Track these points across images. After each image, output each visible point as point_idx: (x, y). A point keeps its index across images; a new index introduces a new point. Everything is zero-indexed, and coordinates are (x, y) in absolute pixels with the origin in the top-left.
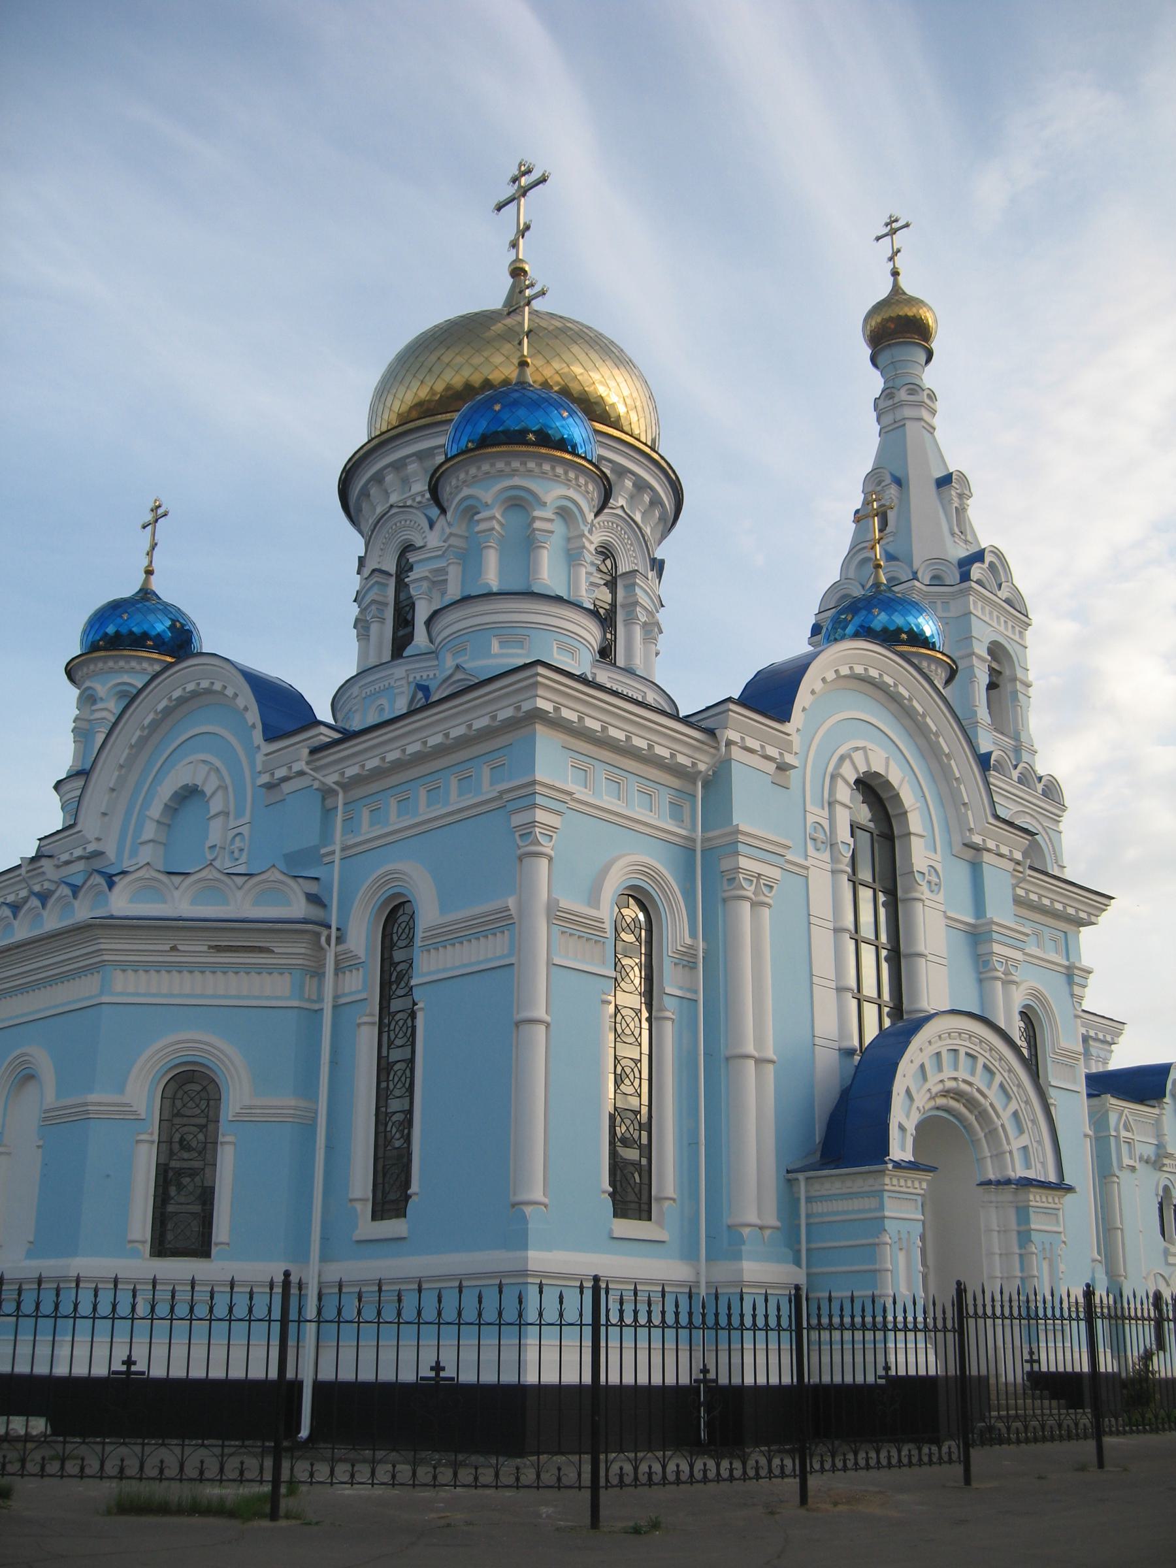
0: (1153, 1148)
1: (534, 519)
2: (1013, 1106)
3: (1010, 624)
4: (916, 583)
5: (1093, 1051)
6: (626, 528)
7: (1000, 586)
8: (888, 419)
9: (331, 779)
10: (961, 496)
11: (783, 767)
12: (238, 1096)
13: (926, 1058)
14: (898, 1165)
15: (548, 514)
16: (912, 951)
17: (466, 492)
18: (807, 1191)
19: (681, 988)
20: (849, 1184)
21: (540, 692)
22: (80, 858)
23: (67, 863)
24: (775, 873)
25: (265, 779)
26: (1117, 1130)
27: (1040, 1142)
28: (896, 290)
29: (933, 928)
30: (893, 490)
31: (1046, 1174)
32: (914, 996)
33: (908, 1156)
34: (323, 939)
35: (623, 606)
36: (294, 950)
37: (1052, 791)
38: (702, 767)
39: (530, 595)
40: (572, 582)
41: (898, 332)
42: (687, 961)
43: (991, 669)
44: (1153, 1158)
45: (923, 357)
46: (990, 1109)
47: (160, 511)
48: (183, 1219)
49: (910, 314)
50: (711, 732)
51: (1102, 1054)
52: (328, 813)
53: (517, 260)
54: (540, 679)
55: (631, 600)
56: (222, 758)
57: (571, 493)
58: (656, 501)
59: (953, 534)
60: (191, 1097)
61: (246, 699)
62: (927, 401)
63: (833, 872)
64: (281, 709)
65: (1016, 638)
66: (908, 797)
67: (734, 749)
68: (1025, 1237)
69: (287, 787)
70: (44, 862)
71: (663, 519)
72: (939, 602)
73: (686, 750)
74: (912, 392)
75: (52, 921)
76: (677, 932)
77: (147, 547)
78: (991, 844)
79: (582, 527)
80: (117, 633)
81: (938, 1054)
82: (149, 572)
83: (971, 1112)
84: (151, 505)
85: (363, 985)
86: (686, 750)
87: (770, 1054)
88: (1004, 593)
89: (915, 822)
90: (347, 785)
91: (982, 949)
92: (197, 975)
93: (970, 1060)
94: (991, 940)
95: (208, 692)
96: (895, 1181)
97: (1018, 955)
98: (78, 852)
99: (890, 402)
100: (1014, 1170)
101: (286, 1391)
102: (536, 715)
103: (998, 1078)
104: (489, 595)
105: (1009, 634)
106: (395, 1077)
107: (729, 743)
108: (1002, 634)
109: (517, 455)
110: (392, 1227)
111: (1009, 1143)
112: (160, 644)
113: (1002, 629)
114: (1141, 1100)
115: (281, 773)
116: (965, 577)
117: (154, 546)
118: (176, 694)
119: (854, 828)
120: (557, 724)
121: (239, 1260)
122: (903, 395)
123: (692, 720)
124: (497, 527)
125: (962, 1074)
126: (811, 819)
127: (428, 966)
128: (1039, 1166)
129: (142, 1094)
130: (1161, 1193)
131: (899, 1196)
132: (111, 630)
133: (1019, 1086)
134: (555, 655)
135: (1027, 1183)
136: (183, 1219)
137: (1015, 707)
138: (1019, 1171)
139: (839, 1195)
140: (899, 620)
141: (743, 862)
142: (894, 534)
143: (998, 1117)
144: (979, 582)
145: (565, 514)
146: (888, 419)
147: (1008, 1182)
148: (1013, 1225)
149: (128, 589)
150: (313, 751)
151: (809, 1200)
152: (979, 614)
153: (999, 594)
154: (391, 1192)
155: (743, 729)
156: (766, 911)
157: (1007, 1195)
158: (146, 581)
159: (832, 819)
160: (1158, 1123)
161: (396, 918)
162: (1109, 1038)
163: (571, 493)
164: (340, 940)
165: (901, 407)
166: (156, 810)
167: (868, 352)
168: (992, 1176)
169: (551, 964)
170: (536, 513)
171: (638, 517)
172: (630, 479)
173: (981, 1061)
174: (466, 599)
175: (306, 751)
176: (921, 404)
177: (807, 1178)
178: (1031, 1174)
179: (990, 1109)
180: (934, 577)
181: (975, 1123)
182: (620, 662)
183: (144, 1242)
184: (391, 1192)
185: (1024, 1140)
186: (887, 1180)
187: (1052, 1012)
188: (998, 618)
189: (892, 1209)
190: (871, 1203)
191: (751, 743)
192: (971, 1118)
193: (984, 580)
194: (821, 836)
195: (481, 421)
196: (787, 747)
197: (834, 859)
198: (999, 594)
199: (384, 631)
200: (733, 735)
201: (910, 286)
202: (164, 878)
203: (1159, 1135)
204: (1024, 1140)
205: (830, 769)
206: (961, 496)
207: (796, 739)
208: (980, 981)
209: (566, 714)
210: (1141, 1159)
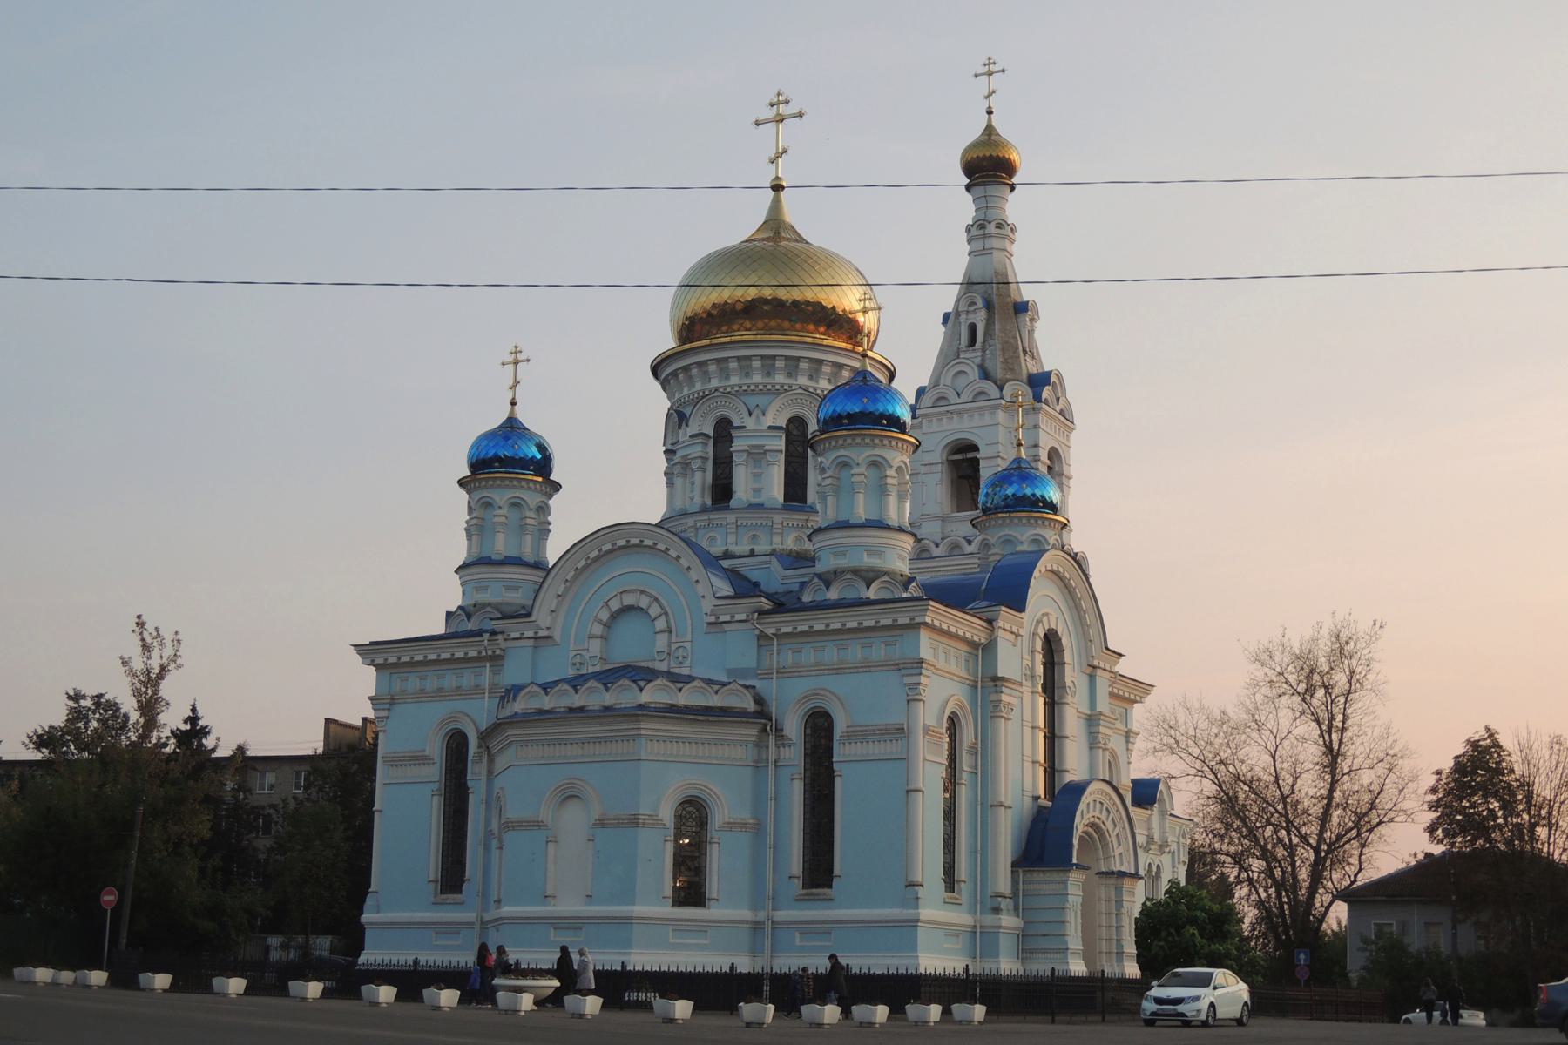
9: (770, 631)
11: (1017, 635)
36: (750, 732)
41: (988, 168)
53: (777, 178)
66: (1065, 642)
74: (999, 226)
76: (967, 736)
77: (511, 383)
82: (513, 404)
89: (1068, 657)
117: (516, 383)
121: (727, 903)
122: (991, 228)
125: (1097, 814)
138: (1117, 867)
139: (1043, 881)
147: (1113, 873)
154: (819, 870)
157: (1112, 881)
158: (512, 411)
165: (987, 231)
176: (1005, 237)
177: (1427, 924)
185: (1121, 850)
191: (1007, 627)
197: (1034, 686)
199: (703, 477)
201: (1003, 129)
204: (1121, 850)
206: (1032, 320)
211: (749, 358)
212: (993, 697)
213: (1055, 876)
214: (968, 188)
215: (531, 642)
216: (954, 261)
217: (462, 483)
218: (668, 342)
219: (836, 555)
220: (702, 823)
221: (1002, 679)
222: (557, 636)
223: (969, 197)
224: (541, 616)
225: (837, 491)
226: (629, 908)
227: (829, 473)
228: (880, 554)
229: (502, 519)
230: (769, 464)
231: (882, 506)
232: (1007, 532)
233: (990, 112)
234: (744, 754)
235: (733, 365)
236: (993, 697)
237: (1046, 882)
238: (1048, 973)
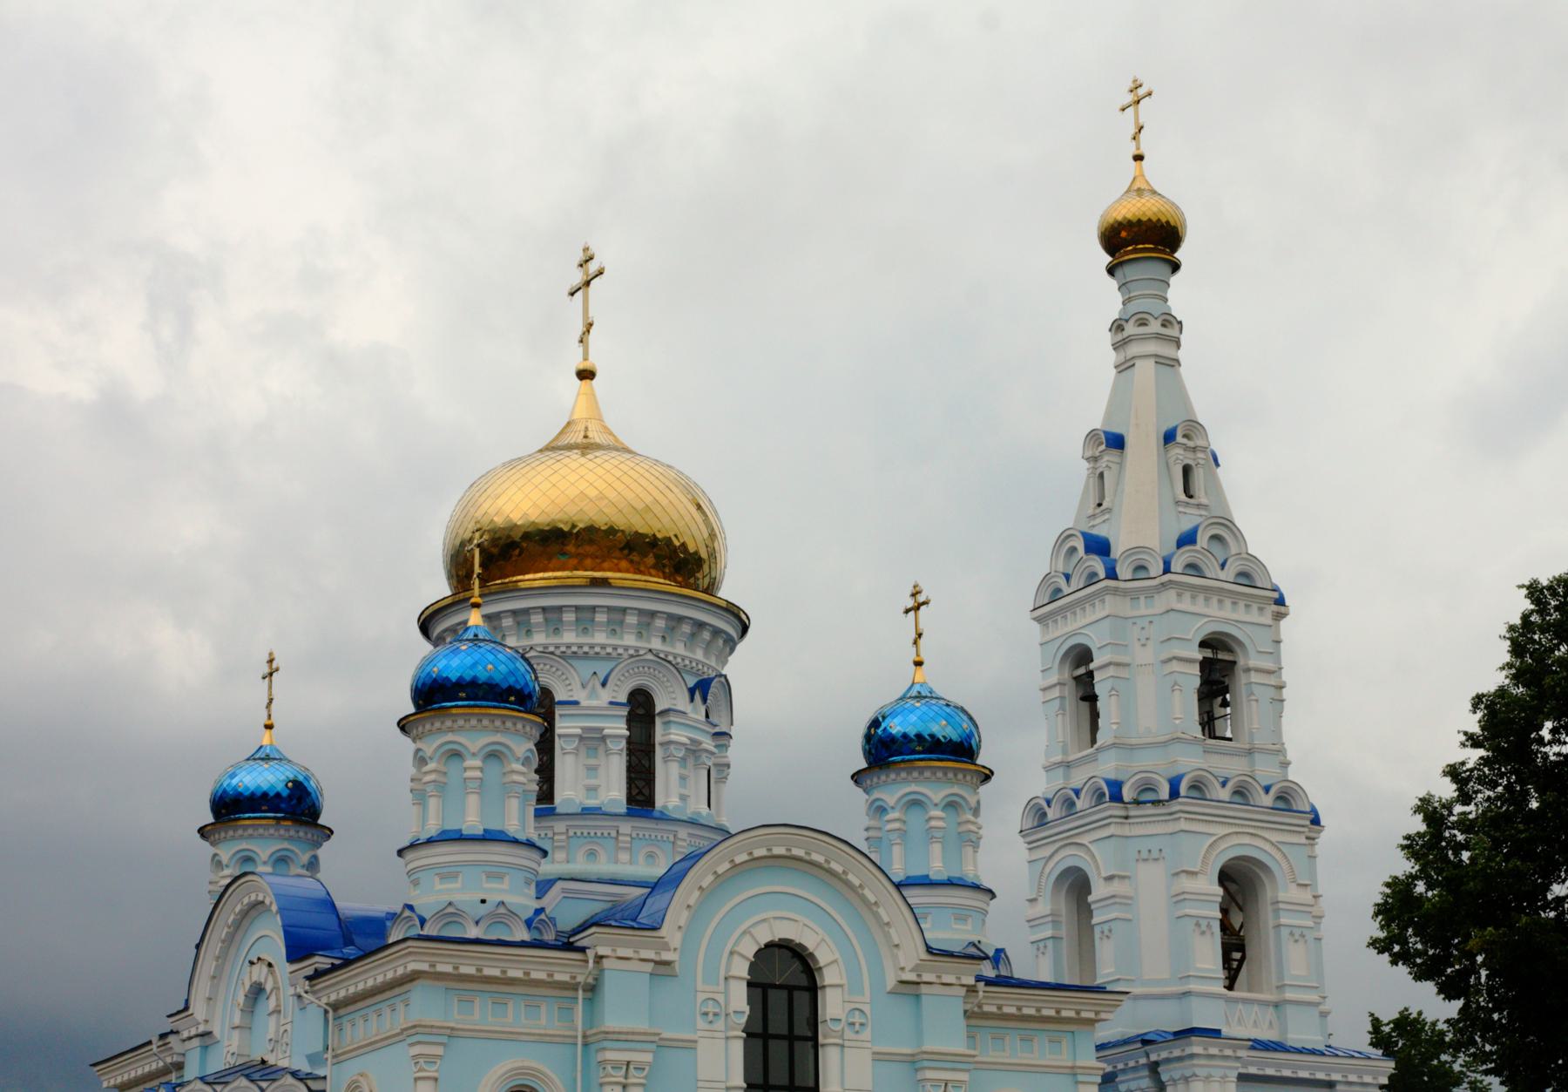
23: (190, 1038)
24: (648, 1057)
28: (1138, 189)
30: (1111, 457)
35: (661, 744)
38: (580, 979)
39: (458, 838)
43: (1205, 665)
66: (823, 956)
67: (606, 963)
70: (171, 1038)
72: (1142, 598)
107: (599, 958)
108: (1227, 621)
142: (1109, 510)
144: (1193, 568)
165: (1147, 335)
166: (241, 999)
191: (621, 952)
196: (666, 947)
200: (602, 951)
211: (560, 609)
214: (1111, 271)
215: (649, 967)
216: (1087, 383)
218: (439, 588)
219: (443, 877)
222: (217, 1033)
223: (1112, 284)
224: (199, 1009)
225: (441, 787)
227: (431, 766)
229: (897, 825)
230: (608, 752)
232: (244, 846)
235: (537, 618)
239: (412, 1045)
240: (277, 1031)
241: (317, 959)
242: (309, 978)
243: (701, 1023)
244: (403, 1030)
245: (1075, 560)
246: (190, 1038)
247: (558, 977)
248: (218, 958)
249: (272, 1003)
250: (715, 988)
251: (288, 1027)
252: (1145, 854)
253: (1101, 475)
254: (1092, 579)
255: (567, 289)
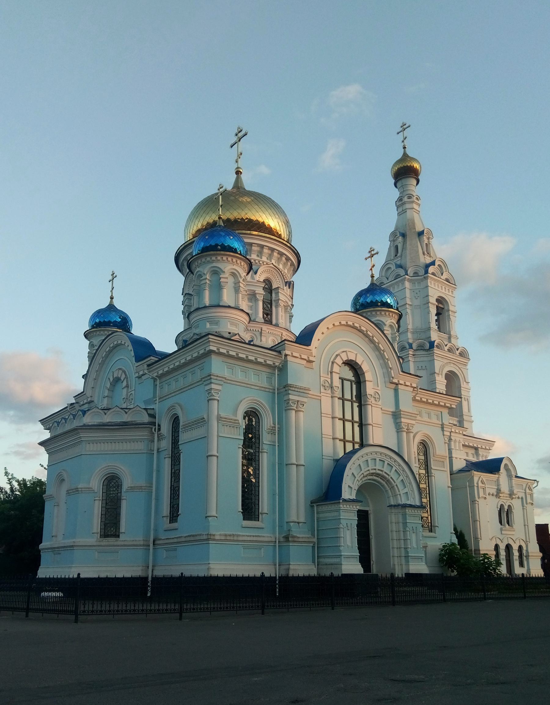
0: (495, 490)
1: (220, 278)
2: (401, 478)
3: (447, 288)
4: (406, 276)
5: (480, 453)
6: (275, 271)
7: (442, 274)
8: (400, 209)
10: (428, 238)
11: (310, 361)
12: (126, 483)
13: (361, 462)
14: (345, 500)
15: (227, 275)
16: (366, 423)
17: (198, 269)
18: (317, 510)
19: (270, 441)
20: (330, 507)
21: (211, 344)
22: (86, 403)
23: (83, 405)
25: (137, 375)
26: (478, 484)
27: (413, 491)
29: (377, 415)
30: (400, 239)
31: (415, 501)
32: (367, 439)
33: (353, 497)
34: (153, 430)
36: (144, 434)
37: (464, 354)
38: (277, 364)
39: (219, 306)
40: (237, 300)
42: (272, 431)
44: (495, 494)
45: (414, 182)
46: (391, 479)
47: (240, 135)
48: (111, 526)
49: (409, 165)
50: (279, 352)
51: (485, 454)
52: (155, 386)
54: (210, 339)
55: (277, 298)
56: (126, 358)
57: (235, 267)
58: (292, 264)
59: (424, 254)
60: (112, 483)
61: (131, 347)
62: (416, 201)
63: (332, 397)
64: (143, 349)
65: (450, 294)
68: (405, 524)
69: (143, 377)
71: (292, 264)
73: (271, 359)
75: (68, 427)
77: (111, 289)
78: (401, 382)
79: (240, 279)
80: (100, 321)
81: (367, 460)
83: (384, 481)
84: (111, 273)
85: (166, 444)
86: (271, 359)
87: (302, 462)
88: (445, 276)
90: (161, 377)
91: (398, 421)
92: (113, 444)
93: (382, 462)
94: (401, 418)
95: (121, 344)
96: (345, 506)
97: (413, 422)
98: (85, 401)
99: (401, 203)
100: (401, 501)
101: (144, 580)
102: (211, 352)
103: (394, 468)
104: (205, 307)
105: (447, 292)
106: (175, 476)
107: (286, 355)
109: (214, 255)
110: (174, 525)
111: (399, 491)
112: (115, 324)
113: (443, 291)
114: (491, 472)
115: (141, 373)
116: (426, 272)
118: (111, 345)
119: (342, 380)
120: (220, 354)
122: (406, 199)
123: (273, 348)
124: (208, 282)
126: (322, 379)
127: (183, 437)
128: (412, 499)
129: (96, 484)
130: (499, 507)
131: (346, 511)
132: (97, 321)
133: (404, 470)
134: (229, 327)
135: (405, 506)
136: (111, 526)
137: (449, 321)
139: (327, 511)
140: (378, 298)
141: (291, 397)
143: (395, 482)
144: (433, 274)
145: (233, 275)
146: (400, 209)
147: (399, 505)
148: (401, 520)
149: (104, 304)
150: (149, 366)
151: (318, 513)
152: (433, 286)
153: (442, 277)
154: (174, 516)
155: (292, 350)
156: (301, 413)
157: (400, 510)
159: (332, 378)
160: (498, 480)
161: (176, 421)
162: (487, 448)
163: (235, 267)
164: (159, 429)
166: (108, 385)
167: (393, 181)
168: (393, 503)
169: (218, 436)
170: (221, 276)
171: (281, 267)
172: (255, 246)
173: (386, 463)
174: (198, 309)
175: (146, 366)
178: (409, 502)
179: (391, 479)
180: (415, 273)
181: (386, 485)
182: (274, 322)
183: (98, 533)
184: (174, 516)
185: (406, 490)
186: (341, 506)
187: (434, 443)
188: (442, 287)
189: (343, 515)
190: (336, 514)
191: (295, 354)
192: (384, 483)
193: (435, 272)
194: (327, 384)
195: (219, 237)
196: (311, 355)
198: (442, 277)
200: (287, 352)
202: (101, 411)
203: (498, 485)
205: (332, 360)
207: (314, 352)
208: (398, 432)
209: (222, 350)
210: (489, 494)
212: (286, 398)
213: (333, 507)
216: (390, 220)
217: (87, 335)
220: (119, 486)
221: (290, 386)
222: (96, 401)
226: (74, 540)
228: (217, 323)
231: (220, 296)
233: (404, 148)
234: (141, 446)
236: (286, 398)
237: (330, 511)
238: (76, 576)
239: (206, 385)
240: (127, 395)
241: (152, 358)
242: (148, 366)
243: (322, 390)
244: (202, 379)
245: (390, 271)
246: (83, 405)
247: (268, 362)
248: (100, 364)
249: (125, 384)
250: (327, 376)
251: (133, 392)
252: (420, 368)
253: (397, 247)
254: (398, 276)
255: (229, 146)
